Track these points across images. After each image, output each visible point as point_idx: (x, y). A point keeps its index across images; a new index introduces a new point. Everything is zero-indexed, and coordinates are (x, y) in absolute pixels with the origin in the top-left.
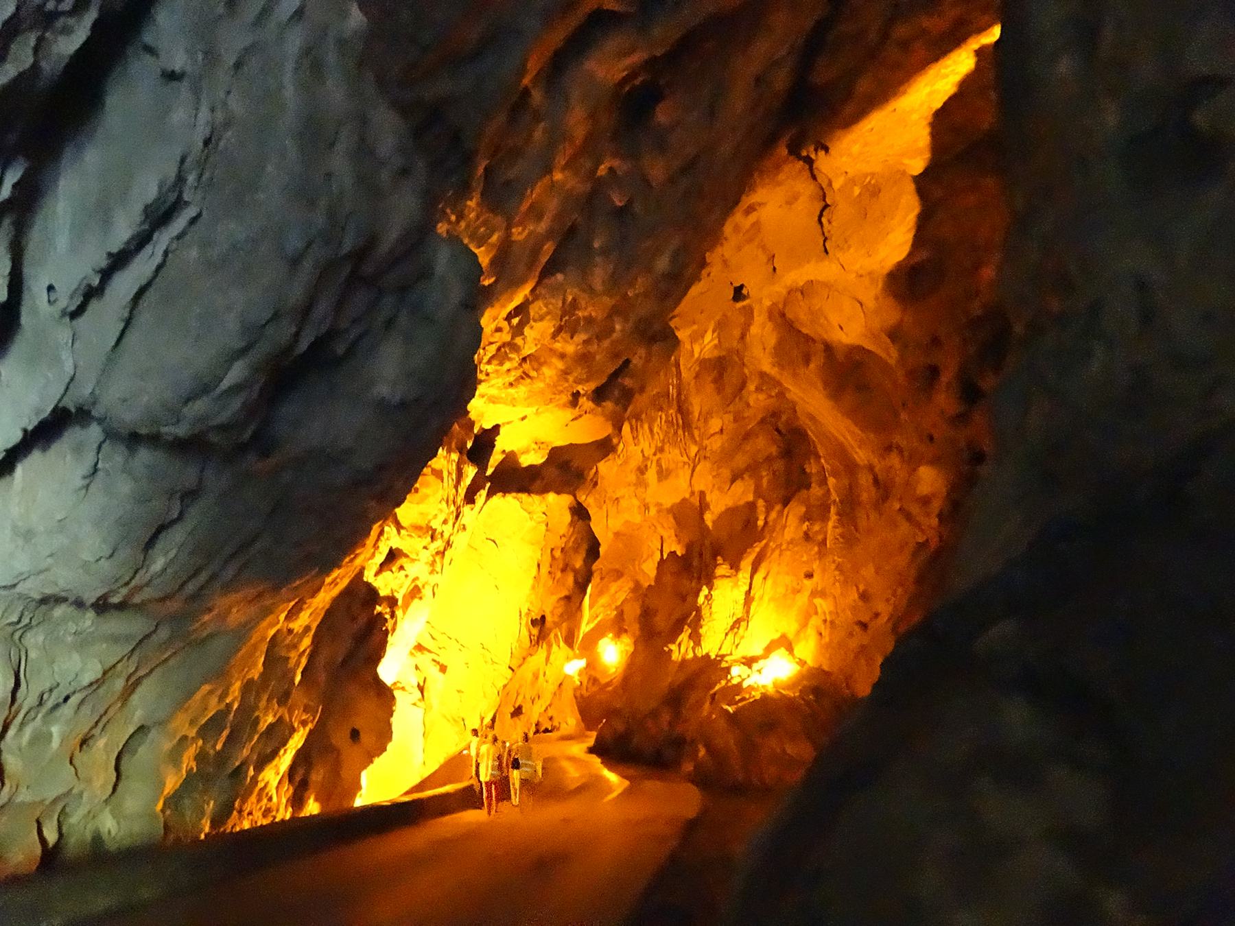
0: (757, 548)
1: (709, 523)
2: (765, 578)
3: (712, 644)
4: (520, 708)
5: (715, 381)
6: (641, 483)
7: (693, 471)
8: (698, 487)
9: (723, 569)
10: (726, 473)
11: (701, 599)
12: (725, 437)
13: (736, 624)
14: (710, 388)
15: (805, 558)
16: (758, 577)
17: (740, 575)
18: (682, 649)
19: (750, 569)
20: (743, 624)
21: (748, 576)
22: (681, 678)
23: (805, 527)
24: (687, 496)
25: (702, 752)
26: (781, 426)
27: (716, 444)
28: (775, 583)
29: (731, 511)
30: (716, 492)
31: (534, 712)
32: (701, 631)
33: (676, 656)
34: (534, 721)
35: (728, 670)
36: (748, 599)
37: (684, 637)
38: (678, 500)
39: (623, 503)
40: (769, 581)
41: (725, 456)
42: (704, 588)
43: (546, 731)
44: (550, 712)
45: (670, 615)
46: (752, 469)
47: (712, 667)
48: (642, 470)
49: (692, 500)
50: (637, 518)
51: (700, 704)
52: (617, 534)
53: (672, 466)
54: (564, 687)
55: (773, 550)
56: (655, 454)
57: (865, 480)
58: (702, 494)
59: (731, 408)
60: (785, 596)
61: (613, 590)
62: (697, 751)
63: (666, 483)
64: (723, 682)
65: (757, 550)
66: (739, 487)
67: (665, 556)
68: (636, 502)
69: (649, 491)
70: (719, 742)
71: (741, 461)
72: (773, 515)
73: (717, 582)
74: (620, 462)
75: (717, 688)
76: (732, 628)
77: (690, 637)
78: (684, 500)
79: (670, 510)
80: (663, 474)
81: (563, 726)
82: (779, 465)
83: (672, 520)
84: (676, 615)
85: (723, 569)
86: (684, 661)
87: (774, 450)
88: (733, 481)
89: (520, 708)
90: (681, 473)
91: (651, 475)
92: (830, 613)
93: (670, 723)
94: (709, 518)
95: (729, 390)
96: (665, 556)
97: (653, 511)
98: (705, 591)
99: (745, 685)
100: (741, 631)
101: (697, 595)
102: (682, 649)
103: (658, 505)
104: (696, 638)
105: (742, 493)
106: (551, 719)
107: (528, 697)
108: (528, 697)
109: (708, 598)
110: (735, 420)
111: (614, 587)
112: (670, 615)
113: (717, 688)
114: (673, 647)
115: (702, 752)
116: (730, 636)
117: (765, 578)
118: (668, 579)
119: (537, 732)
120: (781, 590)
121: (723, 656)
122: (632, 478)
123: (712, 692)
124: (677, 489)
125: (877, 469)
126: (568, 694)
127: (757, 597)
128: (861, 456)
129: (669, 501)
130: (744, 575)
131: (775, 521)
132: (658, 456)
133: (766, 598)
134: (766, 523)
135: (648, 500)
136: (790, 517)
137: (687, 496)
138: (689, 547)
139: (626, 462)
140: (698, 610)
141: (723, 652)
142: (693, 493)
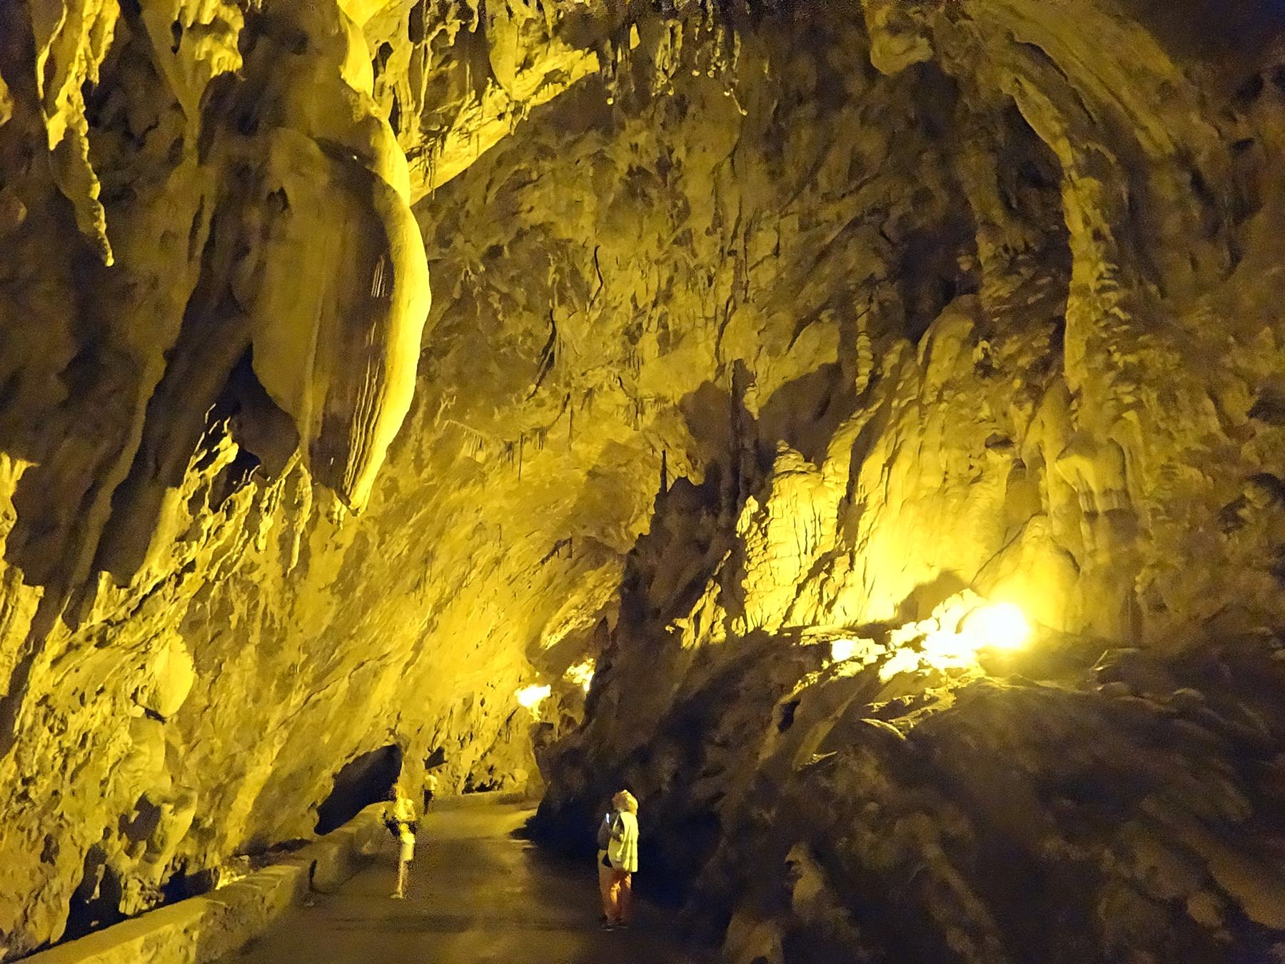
0: (861, 419)
1: (754, 410)
2: (890, 463)
3: (772, 598)
4: (440, 751)
5: (767, 157)
6: (630, 360)
7: (721, 332)
8: (732, 353)
9: (789, 461)
10: (784, 319)
11: (743, 523)
12: (782, 261)
13: (824, 565)
14: (756, 172)
15: (985, 412)
16: (873, 465)
17: (828, 469)
18: (702, 626)
19: (848, 456)
20: (842, 563)
21: (844, 469)
22: (700, 681)
23: (978, 354)
24: (711, 376)
25: (808, 885)
26: (889, 229)
27: (765, 276)
28: (917, 469)
29: (791, 388)
30: (765, 358)
31: (466, 760)
32: (744, 583)
33: (688, 640)
34: (463, 775)
35: (823, 649)
36: (849, 511)
37: (706, 602)
38: (696, 387)
39: (602, 402)
40: (903, 465)
41: (789, 288)
42: (751, 500)
43: (482, 788)
44: (490, 760)
45: (677, 577)
46: (842, 304)
47: (785, 652)
48: (632, 335)
49: (718, 384)
50: (626, 434)
51: (747, 736)
52: (592, 474)
53: (687, 326)
54: (513, 724)
55: (902, 412)
56: (655, 305)
57: (1166, 186)
58: (739, 363)
59: (796, 206)
60: (943, 492)
61: (590, 582)
62: (788, 873)
63: (672, 357)
64: (813, 677)
65: (862, 422)
66: (809, 340)
67: (669, 486)
68: (620, 397)
69: (644, 373)
70: (871, 847)
71: (813, 293)
72: (892, 359)
73: (781, 485)
74: (595, 316)
75: (797, 689)
76: (813, 573)
77: (719, 601)
78: (705, 385)
79: (681, 407)
80: (668, 342)
81: (509, 780)
82: (890, 293)
83: (683, 430)
84: (688, 576)
85: (789, 461)
86: (706, 651)
87: (878, 268)
88: (800, 326)
89: (440, 751)
90: (700, 334)
91: (648, 344)
92: (1107, 493)
93: (676, 776)
94: (753, 402)
95: (792, 174)
96: (669, 486)
97: (651, 412)
98: (752, 505)
99: (885, 674)
100: (838, 573)
101: (735, 513)
102: (702, 626)
103: (660, 399)
104: (734, 601)
105: (815, 349)
106: (491, 770)
107: (454, 735)
108: (454, 735)
109: (761, 518)
110: (803, 228)
111: (591, 578)
112: (677, 577)
113: (797, 689)
114: (682, 623)
115: (808, 885)
116: (813, 586)
117: (890, 463)
118: (673, 522)
119: (468, 789)
120: (933, 481)
121: (797, 631)
122: (614, 348)
123: (787, 699)
124: (698, 364)
125: (1201, 160)
126: (521, 734)
127: (872, 501)
128: (1156, 133)
129: (677, 391)
130: (837, 468)
131: (897, 369)
132: (661, 308)
133: (895, 501)
134: (874, 379)
135: (644, 392)
136: (939, 343)
137: (711, 376)
138: (713, 473)
139: (603, 320)
140: (738, 548)
141: (796, 621)
142: (721, 370)
